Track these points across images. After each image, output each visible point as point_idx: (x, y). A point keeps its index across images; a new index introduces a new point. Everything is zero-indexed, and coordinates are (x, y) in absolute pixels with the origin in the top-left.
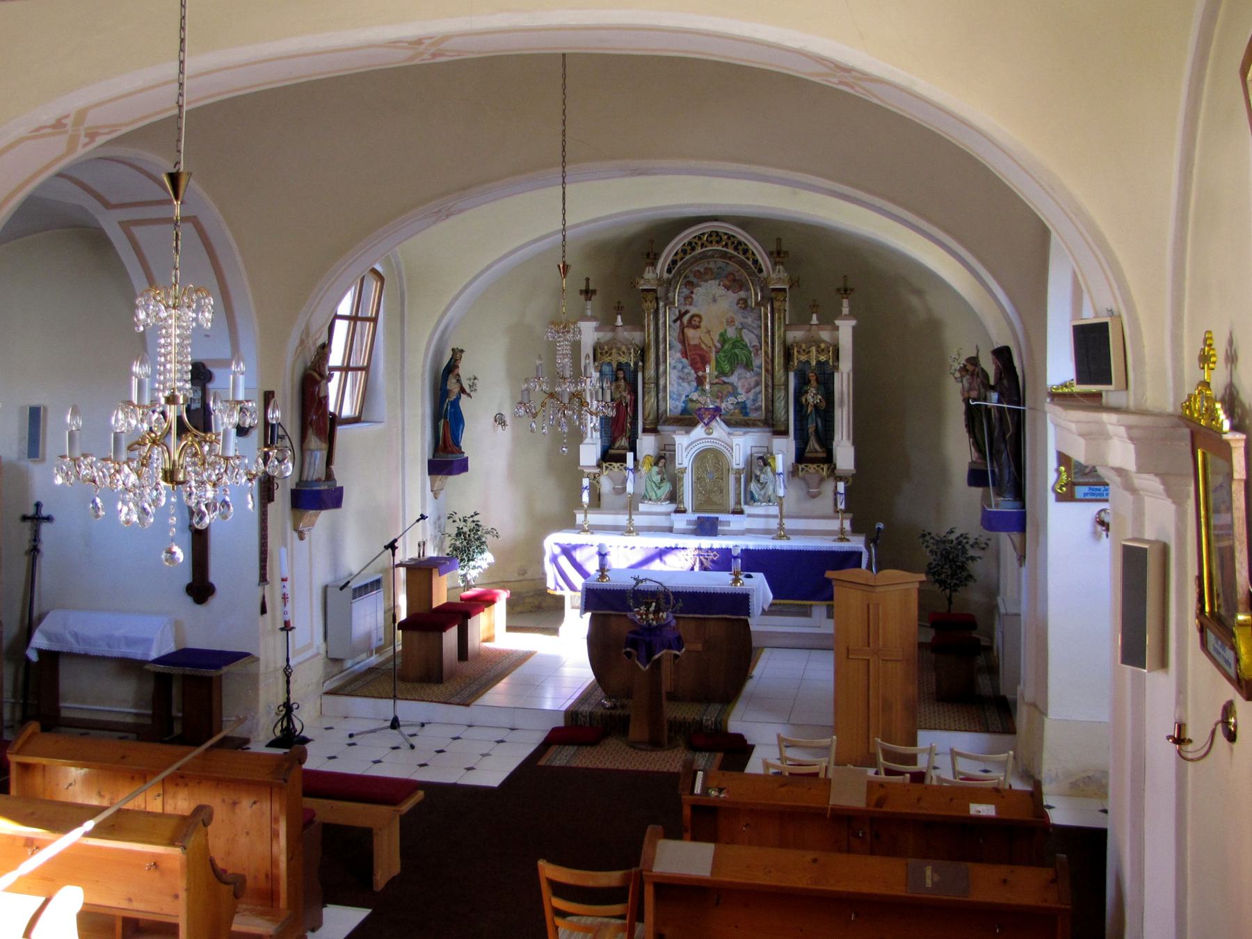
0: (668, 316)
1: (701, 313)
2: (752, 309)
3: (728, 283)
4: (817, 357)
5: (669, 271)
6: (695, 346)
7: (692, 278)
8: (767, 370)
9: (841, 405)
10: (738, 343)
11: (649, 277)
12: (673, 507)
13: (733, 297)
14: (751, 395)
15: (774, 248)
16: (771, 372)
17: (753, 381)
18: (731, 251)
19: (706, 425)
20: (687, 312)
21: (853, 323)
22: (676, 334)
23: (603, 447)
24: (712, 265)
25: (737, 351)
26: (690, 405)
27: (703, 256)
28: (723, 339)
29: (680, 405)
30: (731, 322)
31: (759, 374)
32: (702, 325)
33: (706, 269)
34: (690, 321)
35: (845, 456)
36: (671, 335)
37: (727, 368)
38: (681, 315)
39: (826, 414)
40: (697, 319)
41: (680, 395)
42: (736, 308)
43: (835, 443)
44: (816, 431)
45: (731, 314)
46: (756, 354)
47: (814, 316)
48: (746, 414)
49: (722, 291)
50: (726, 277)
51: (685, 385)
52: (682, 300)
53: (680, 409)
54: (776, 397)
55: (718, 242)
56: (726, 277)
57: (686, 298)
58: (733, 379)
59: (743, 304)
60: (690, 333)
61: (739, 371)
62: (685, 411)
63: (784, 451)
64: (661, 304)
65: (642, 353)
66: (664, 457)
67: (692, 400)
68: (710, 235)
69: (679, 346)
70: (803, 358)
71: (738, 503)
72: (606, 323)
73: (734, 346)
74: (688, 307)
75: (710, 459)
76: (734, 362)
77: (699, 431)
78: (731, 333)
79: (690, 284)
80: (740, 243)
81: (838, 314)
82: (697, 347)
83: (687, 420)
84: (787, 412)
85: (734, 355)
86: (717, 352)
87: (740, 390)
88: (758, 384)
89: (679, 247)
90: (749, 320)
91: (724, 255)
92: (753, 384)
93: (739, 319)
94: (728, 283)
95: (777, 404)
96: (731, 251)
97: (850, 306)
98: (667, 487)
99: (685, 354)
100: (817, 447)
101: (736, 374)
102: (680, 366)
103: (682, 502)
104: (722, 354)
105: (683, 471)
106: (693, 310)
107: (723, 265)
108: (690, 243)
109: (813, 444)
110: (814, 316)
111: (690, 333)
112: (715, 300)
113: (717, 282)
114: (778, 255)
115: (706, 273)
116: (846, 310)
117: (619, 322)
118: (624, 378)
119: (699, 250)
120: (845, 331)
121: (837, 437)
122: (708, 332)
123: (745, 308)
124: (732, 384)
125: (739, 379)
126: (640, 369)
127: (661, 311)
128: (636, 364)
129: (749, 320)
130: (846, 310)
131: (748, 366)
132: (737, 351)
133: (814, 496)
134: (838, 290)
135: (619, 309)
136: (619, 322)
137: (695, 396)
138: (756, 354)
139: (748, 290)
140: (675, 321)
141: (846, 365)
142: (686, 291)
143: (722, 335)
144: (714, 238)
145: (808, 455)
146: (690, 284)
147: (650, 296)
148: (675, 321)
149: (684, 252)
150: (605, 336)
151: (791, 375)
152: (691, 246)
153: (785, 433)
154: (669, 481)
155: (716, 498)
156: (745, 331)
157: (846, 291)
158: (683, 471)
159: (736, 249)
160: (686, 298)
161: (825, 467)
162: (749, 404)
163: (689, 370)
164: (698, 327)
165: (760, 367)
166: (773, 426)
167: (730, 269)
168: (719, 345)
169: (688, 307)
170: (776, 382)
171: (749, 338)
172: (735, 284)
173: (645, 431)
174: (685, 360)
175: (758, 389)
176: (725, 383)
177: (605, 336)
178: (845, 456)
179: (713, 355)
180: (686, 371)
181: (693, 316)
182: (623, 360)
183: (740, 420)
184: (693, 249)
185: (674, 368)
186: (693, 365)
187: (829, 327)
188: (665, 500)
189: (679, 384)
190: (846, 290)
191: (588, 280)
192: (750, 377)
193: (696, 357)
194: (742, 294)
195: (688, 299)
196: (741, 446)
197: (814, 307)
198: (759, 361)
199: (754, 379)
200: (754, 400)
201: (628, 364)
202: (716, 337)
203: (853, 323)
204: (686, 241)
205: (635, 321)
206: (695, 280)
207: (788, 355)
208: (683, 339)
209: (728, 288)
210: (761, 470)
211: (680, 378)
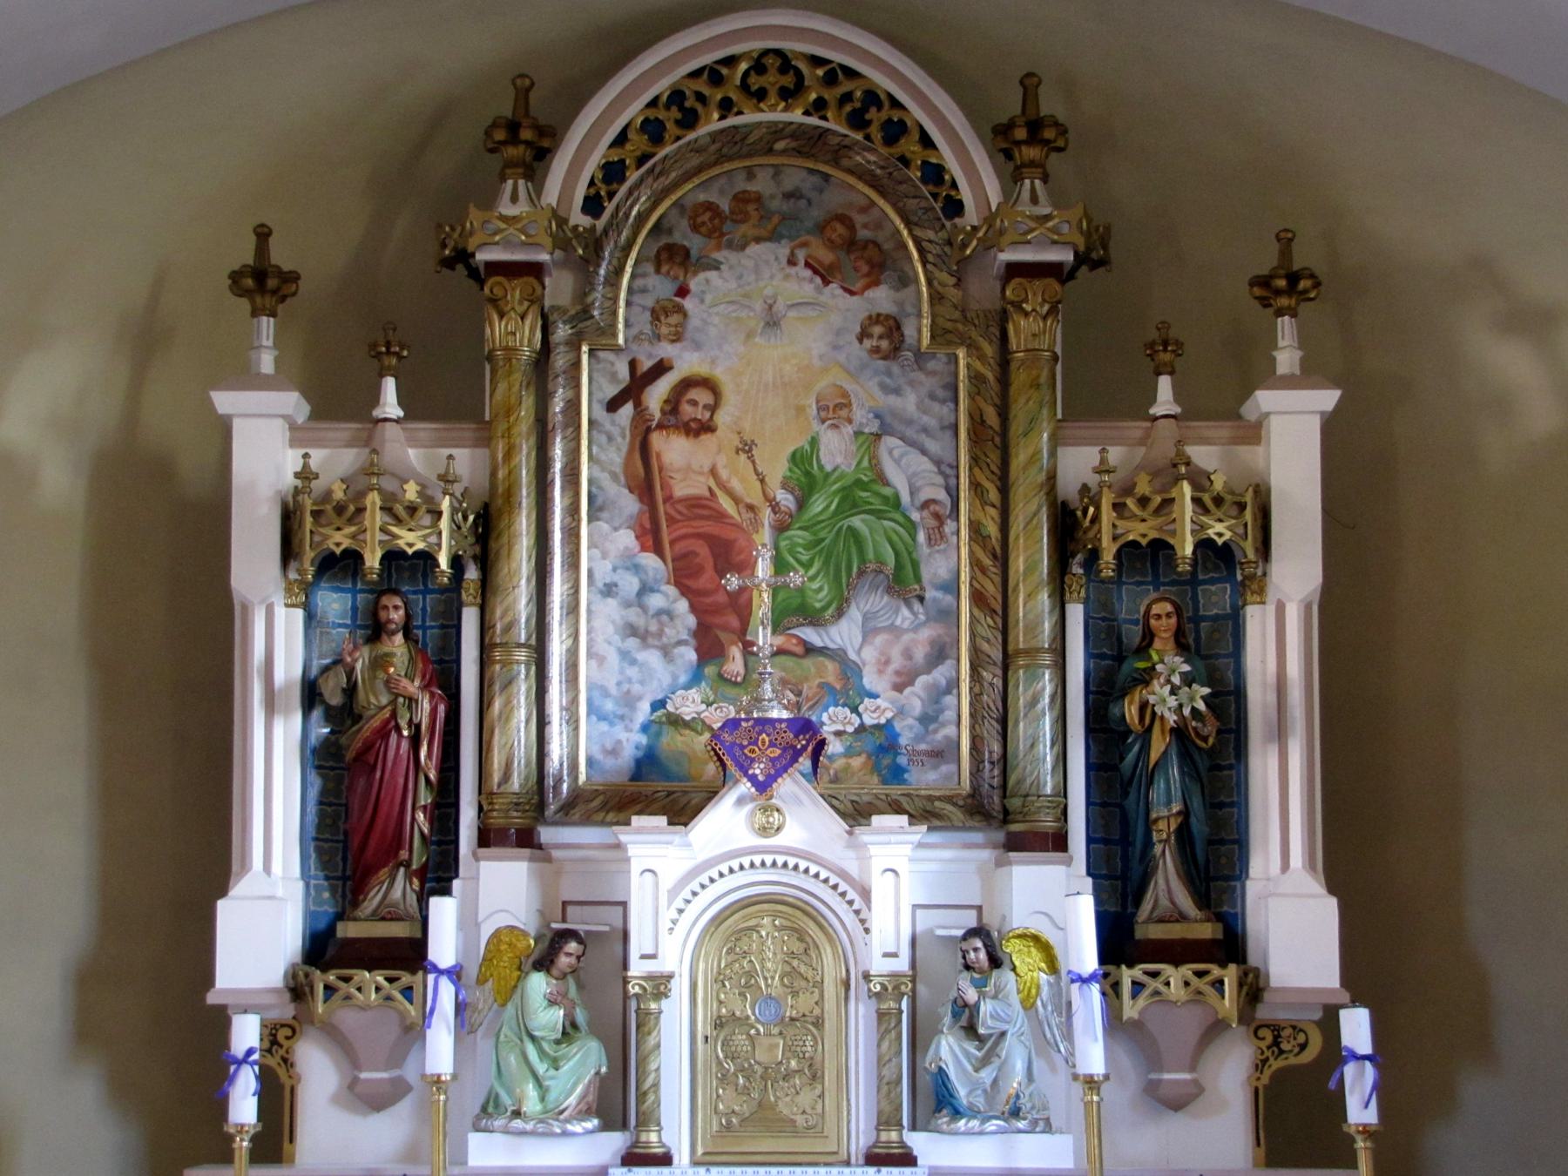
0: (593, 383)
1: (719, 373)
2: (919, 356)
3: (825, 256)
4: (1200, 527)
5: (593, 205)
6: (694, 503)
7: (683, 235)
8: (978, 598)
9: (1280, 733)
10: (865, 492)
11: (511, 225)
12: (616, 1141)
13: (845, 308)
14: (915, 699)
15: (1010, 105)
16: (996, 606)
17: (921, 640)
18: (835, 124)
19: (763, 787)
20: (661, 368)
21: (1328, 399)
22: (615, 456)
23: (309, 916)
24: (762, 184)
25: (857, 522)
26: (673, 741)
27: (734, 144)
28: (806, 475)
29: (631, 741)
30: (835, 409)
31: (949, 616)
32: (722, 418)
33: (741, 199)
34: (673, 404)
35: (1295, 926)
36: (596, 455)
37: (820, 592)
38: (634, 389)
39: (1216, 754)
40: (702, 396)
41: (629, 701)
42: (858, 351)
43: (1253, 888)
44: (1184, 835)
45: (838, 377)
46: (937, 536)
47: (1165, 384)
48: (896, 774)
49: (801, 285)
50: (821, 228)
51: (652, 658)
52: (643, 321)
53: (629, 754)
54: (1020, 697)
55: (788, 95)
56: (821, 228)
57: (657, 314)
58: (844, 634)
59: (886, 336)
60: (673, 450)
61: (870, 601)
62: (647, 764)
63: (1057, 902)
64: (562, 332)
65: (485, 528)
66: (575, 948)
67: (676, 721)
68: (759, 67)
69: (630, 504)
70: (1141, 530)
71: (887, 1120)
72: (336, 401)
73: (849, 502)
74: (666, 350)
75: (778, 929)
76: (850, 568)
77: (726, 822)
78: (836, 451)
79: (673, 258)
80: (873, 97)
81: (1253, 370)
82: (700, 506)
83: (663, 789)
84: (1062, 759)
85: (852, 543)
86: (780, 528)
87: (870, 680)
88: (940, 653)
89: (634, 111)
90: (909, 403)
91: (809, 143)
92: (920, 654)
93: (867, 396)
94: (825, 256)
95: (1021, 731)
96: (835, 124)
97: (1303, 342)
98: (585, 1062)
99: (650, 537)
100: (1185, 902)
101: (855, 613)
102: (630, 584)
103: (648, 1119)
104: (798, 535)
105: (660, 985)
106: (687, 362)
107: (806, 183)
108: (677, 96)
109: (1168, 885)
110: (1165, 384)
111: (673, 450)
112: (772, 323)
113: (783, 250)
114: (1025, 138)
115: (739, 216)
116: (1287, 359)
117: (390, 404)
118: (407, 630)
119: (712, 124)
120: (1291, 437)
121: (1263, 863)
122: (747, 448)
123: (894, 353)
124: (838, 656)
125: (868, 633)
126: (470, 592)
127: (560, 361)
128: (457, 562)
129: (909, 403)
130: (1287, 359)
131: (902, 582)
132: (857, 522)
133: (1177, 1102)
134: (1263, 282)
135: (383, 352)
136: (390, 404)
137: (689, 704)
138: (937, 536)
139: (905, 281)
140: (613, 405)
141: (1296, 571)
142: (660, 287)
143: (799, 459)
144: (772, 80)
145: (1149, 931)
146: (673, 258)
147: (515, 292)
148: (613, 405)
149: (653, 130)
150: (335, 461)
151: (1076, 614)
152: (681, 107)
153: (1059, 842)
154: (597, 1031)
155: (793, 1102)
156: (890, 441)
157: (1285, 286)
158: (660, 985)
159: (857, 121)
160: (657, 314)
161: (1230, 975)
162: (907, 733)
163: (667, 597)
164: (707, 428)
165: (952, 587)
166: (1006, 817)
167: (834, 199)
168: (786, 500)
169: (666, 350)
170: (1020, 640)
171: (908, 472)
172: (853, 256)
173: (486, 838)
174: (650, 561)
175: (941, 674)
176: (809, 650)
177: (335, 461)
178: (1295, 926)
179: (765, 536)
180: (656, 601)
181: (687, 384)
182: (411, 540)
183: (876, 787)
184: (689, 120)
185: (609, 590)
186: (684, 577)
187: (1223, 430)
188: (584, 1113)
189: (625, 655)
190: (1293, 278)
191: (263, 235)
192: (912, 629)
193: (693, 545)
194: (882, 298)
195: (668, 316)
196: (902, 883)
197: (1163, 351)
198: (949, 562)
199: (926, 633)
200: (927, 720)
201: (426, 559)
202: (777, 469)
203: (1328, 399)
204: (662, 86)
205: (446, 400)
206: (695, 243)
207: (1068, 528)
208: (645, 478)
209: (825, 274)
210: (979, 985)
211: (632, 631)
